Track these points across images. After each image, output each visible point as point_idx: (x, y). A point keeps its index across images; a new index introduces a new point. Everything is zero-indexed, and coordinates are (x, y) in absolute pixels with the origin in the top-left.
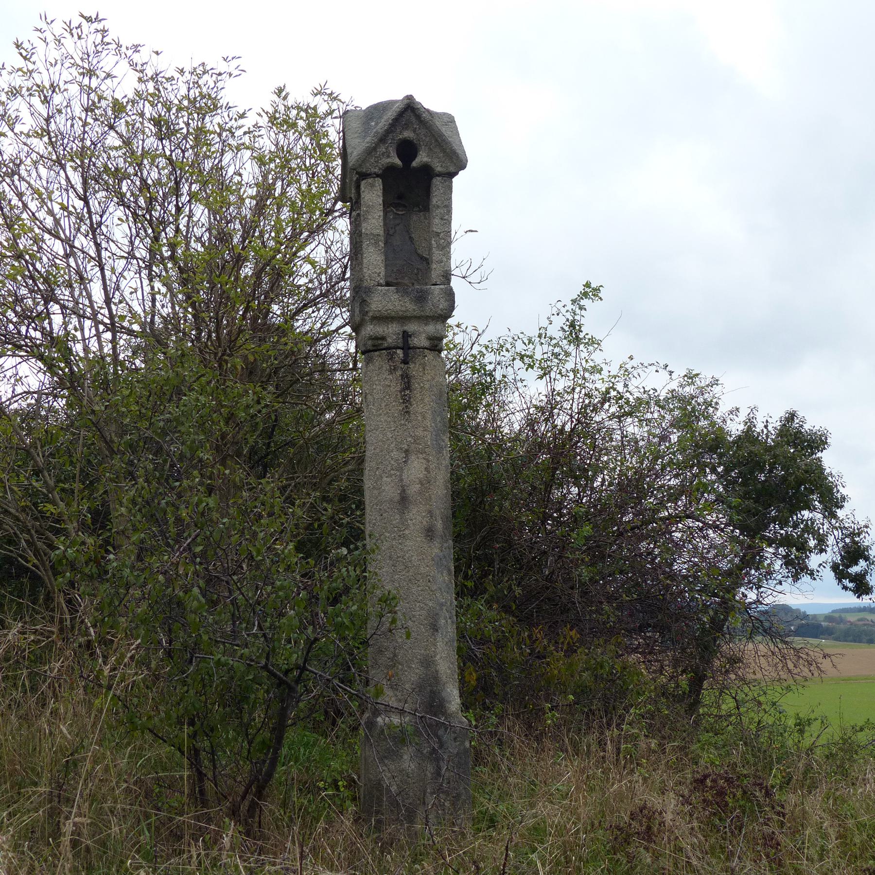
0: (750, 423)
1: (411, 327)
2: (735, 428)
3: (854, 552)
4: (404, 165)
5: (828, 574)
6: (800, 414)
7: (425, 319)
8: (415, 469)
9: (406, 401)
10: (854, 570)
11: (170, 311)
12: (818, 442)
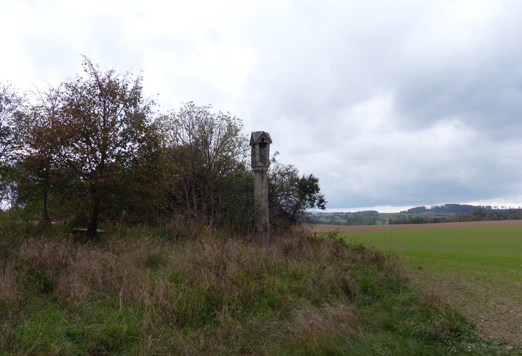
0: (304, 176)
1: (263, 168)
2: (301, 177)
3: (322, 201)
4: (261, 142)
5: (317, 206)
6: (313, 175)
7: (265, 167)
8: (264, 191)
9: (262, 180)
10: (321, 204)
11: (304, 352)
12: (316, 180)
